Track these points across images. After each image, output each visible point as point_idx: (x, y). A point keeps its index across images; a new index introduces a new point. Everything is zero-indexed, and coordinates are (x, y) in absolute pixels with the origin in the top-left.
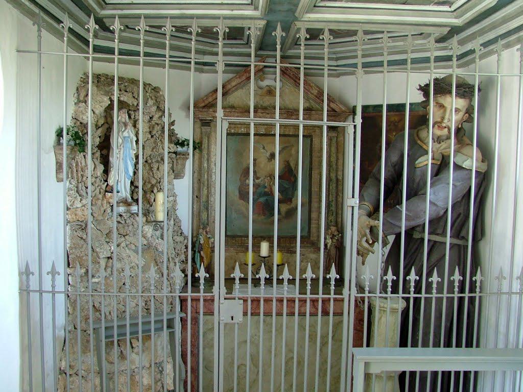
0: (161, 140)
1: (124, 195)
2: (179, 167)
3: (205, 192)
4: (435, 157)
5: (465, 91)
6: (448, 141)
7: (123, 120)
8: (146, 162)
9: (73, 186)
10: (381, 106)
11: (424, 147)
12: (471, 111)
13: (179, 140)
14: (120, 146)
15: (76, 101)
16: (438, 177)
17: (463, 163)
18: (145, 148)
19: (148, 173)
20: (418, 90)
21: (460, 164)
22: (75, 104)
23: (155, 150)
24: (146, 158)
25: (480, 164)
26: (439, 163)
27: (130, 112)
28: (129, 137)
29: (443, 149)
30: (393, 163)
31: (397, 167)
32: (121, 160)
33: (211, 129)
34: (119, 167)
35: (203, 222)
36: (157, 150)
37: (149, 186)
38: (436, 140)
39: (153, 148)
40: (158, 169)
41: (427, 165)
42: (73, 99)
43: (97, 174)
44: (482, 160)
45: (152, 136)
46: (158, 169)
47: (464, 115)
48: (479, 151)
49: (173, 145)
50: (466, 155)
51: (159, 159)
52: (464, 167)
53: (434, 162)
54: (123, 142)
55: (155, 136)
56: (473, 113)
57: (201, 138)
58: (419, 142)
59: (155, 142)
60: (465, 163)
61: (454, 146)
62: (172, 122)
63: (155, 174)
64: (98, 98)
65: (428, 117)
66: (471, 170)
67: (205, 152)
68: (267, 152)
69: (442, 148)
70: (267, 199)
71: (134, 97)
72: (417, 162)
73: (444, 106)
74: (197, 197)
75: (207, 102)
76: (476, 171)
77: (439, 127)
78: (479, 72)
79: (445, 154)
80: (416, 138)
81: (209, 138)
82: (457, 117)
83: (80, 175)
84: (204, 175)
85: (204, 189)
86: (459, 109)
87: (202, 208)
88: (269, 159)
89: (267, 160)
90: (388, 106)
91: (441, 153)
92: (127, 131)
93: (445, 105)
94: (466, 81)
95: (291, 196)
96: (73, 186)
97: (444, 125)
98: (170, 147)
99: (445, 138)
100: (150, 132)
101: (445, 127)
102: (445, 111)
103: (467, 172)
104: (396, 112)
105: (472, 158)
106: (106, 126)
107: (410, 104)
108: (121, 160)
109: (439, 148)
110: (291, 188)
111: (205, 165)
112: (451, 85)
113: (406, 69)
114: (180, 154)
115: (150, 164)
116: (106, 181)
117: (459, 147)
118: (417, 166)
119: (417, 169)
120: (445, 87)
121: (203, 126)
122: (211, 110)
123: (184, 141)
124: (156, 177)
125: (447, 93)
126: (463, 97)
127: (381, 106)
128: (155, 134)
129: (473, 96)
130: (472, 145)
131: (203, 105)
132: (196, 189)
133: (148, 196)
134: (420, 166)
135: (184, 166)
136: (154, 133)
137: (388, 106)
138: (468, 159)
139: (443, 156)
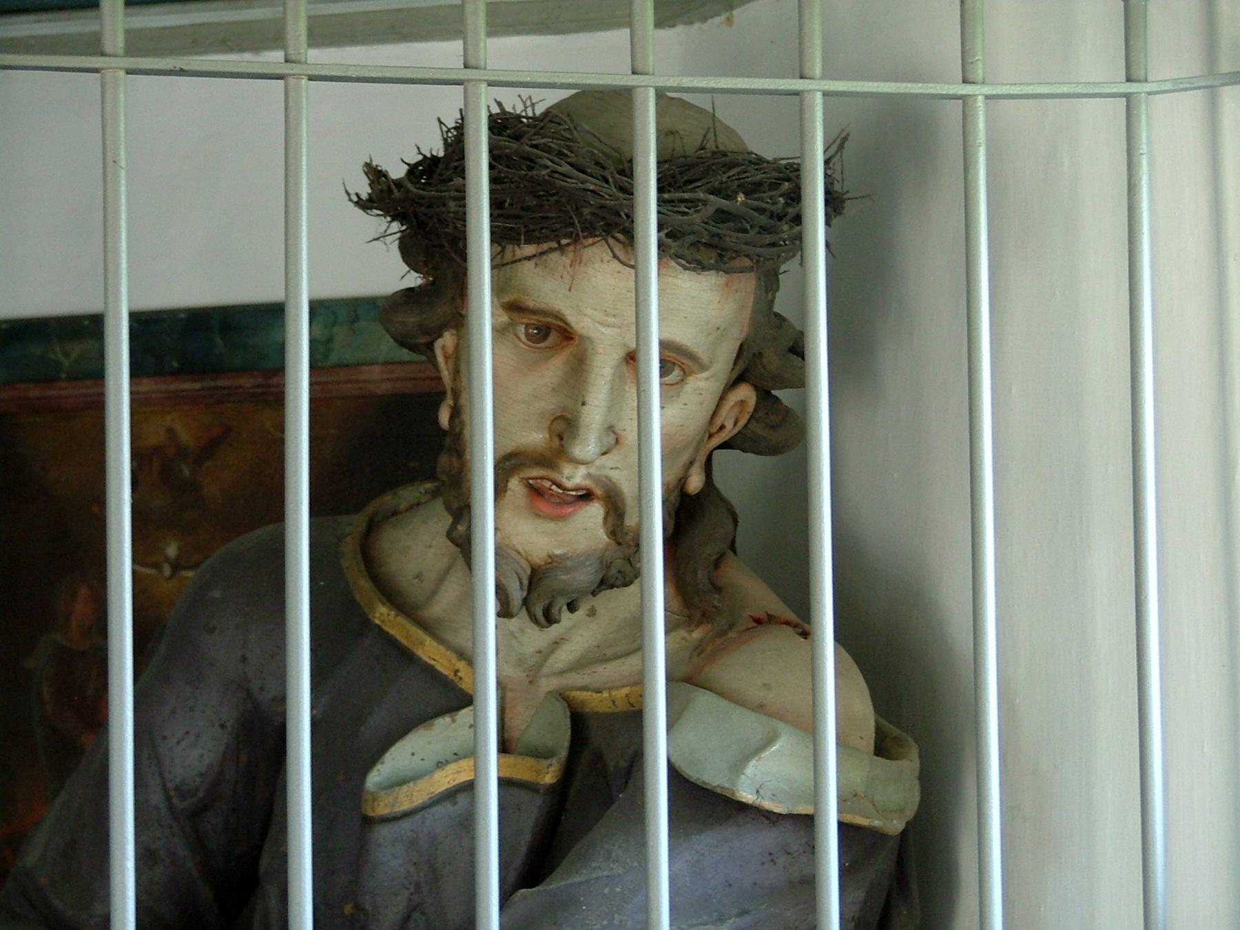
4: (517, 724)
5: (723, 216)
6: (617, 602)
10: (275, 313)
11: (430, 652)
12: (772, 360)
16: (554, 884)
17: (738, 767)
20: (364, 205)
21: (711, 775)
25: (869, 768)
26: (549, 777)
29: (578, 665)
30: (182, 791)
31: (213, 822)
38: (517, 595)
41: (469, 788)
44: (881, 737)
47: (722, 398)
48: (856, 670)
50: (760, 708)
52: (747, 796)
53: (523, 769)
56: (800, 381)
58: (382, 615)
60: (752, 769)
61: (667, 632)
65: (444, 417)
66: (807, 823)
69: (564, 656)
72: (375, 778)
73: (567, 334)
76: (841, 825)
77: (536, 492)
78: (826, 76)
79: (596, 702)
80: (363, 587)
82: (675, 410)
86: (692, 356)
90: (142, 323)
91: (562, 696)
93: (581, 322)
94: (730, 131)
97: (575, 477)
99: (585, 576)
101: (586, 496)
102: (579, 368)
103: (768, 838)
104: (176, 374)
105: (810, 727)
107: (135, 317)
109: (545, 655)
112: (626, 170)
113: (93, 46)
117: (699, 649)
118: (382, 809)
119: (384, 833)
120: (576, 181)
125: (590, 230)
126: (711, 257)
127: (275, 313)
129: (797, 243)
130: (805, 630)
134: (406, 806)
137: (142, 323)
138: (770, 740)
139: (579, 721)
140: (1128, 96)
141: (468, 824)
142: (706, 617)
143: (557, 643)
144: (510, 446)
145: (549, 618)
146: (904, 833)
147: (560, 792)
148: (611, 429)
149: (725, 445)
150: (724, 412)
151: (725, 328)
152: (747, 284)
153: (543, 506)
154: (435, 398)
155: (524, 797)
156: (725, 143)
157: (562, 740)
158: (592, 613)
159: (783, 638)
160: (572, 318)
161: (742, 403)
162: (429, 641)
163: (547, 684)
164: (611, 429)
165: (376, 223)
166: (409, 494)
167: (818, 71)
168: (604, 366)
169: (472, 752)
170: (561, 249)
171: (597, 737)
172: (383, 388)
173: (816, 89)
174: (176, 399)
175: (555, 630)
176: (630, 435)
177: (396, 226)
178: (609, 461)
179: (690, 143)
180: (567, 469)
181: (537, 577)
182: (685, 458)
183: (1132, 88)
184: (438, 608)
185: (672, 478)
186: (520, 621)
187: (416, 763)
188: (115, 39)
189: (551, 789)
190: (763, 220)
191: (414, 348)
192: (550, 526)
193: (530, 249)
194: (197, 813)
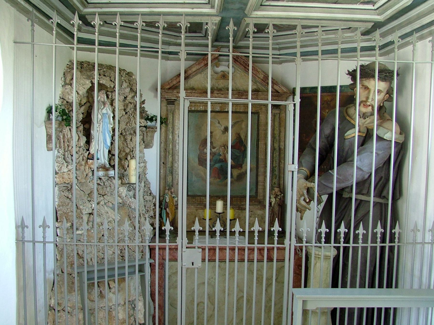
0: (133, 116)
2: (149, 138)
5: (386, 76)
6: (372, 117)
7: (102, 100)
8: (121, 134)
11: (352, 122)
13: (148, 116)
14: (100, 121)
15: (63, 84)
16: (363, 147)
17: (384, 135)
19: (123, 144)
20: (347, 74)
21: (381, 136)
22: (62, 86)
23: (128, 125)
24: (122, 131)
25: (398, 136)
26: (364, 135)
29: (368, 124)
31: (329, 138)
32: (101, 134)
33: (175, 107)
34: (99, 139)
36: (130, 124)
37: (124, 154)
39: (127, 123)
40: (131, 140)
41: (354, 137)
42: (61, 82)
45: (126, 113)
46: (131, 140)
47: (385, 96)
48: (398, 125)
50: (387, 129)
51: (132, 132)
52: (385, 138)
53: (360, 134)
55: (128, 113)
56: (393, 94)
58: (348, 118)
59: (129, 118)
61: (377, 121)
62: (143, 101)
63: (128, 145)
64: (82, 82)
66: (391, 141)
67: (170, 126)
68: (222, 126)
69: (367, 123)
70: (221, 165)
71: (111, 81)
72: (346, 135)
73: (368, 88)
74: (163, 163)
76: (395, 142)
77: (364, 105)
78: (397, 60)
79: (370, 128)
80: (346, 115)
83: (66, 145)
84: (170, 145)
85: (169, 157)
86: (381, 91)
87: (168, 172)
88: (223, 132)
89: (221, 133)
90: (322, 88)
91: (366, 127)
92: (105, 108)
95: (241, 163)
97: (368, 104)
98: (141, 122)
99: (369, 114)
100: (125, 110)
101: (370, 106)
104: (328, 93)
108: (101, 134)
109: (365, 122)
110: (242, 157)
111: (171, 137)
112: (374, 71)
113: (337, 57)
114: (149, 128)
115: (124, 136)
116: (88, 150)
117: (381, 122)
118: (346, 138)
120: (370, 72)
123: (153, 117)
124: (129, 147)
125: (371, 77)
126: (384, 80)
128: (129, 111)
129: (393, 79)
131: (168, 87)
133: (123, 162)
135: (152, 137)
136: (128, 110)
137: (322, 88)
140: (431, 63)
141: (354, 140)
142: (382, 119)
143: (366, 121)
144: (361, 100)
145: (365, 119)
146: (402, 143)
147: (365, 137)
148: (372, 99)
149: (385, 101)
150: (385, 97)
151: (123, 83)
152: (388, 83)
153: (365, 107)
154: (354, 96)
155: (361, 137)
156: (386, 68)
157: (366, 131)
158: (370, 118)
159: (390, 122)
160: (369, 86)
161: (387, 96)
162: (352, 121)
163: (365, 126)
164: (372, 99)
165: (348, 76)
166: (351, 105)
167: (396, 60)
168: (372, 92)
169: (355, 133)
170: (368, 79)
171: (369, 131)
172: (349, 95)
173: (396, 62)
174: (329, 95)
175: (366, 120)
176: (374, 98)
177: (350, 77)
178: (372, 102)
179: (382, 68)
180: (368, 103)
181: (364, 114)
182: (380, 102)
183: (432, 62)
184: (353, 117)
185: (379, 104)
186: (362, 119)
187: (350, 133)
188: (339, 56)
189: (364, 137)
190: (390, 76)
191: (352, 90)
192: (365, 109)
193: (365, 79)
194: (328, 137)
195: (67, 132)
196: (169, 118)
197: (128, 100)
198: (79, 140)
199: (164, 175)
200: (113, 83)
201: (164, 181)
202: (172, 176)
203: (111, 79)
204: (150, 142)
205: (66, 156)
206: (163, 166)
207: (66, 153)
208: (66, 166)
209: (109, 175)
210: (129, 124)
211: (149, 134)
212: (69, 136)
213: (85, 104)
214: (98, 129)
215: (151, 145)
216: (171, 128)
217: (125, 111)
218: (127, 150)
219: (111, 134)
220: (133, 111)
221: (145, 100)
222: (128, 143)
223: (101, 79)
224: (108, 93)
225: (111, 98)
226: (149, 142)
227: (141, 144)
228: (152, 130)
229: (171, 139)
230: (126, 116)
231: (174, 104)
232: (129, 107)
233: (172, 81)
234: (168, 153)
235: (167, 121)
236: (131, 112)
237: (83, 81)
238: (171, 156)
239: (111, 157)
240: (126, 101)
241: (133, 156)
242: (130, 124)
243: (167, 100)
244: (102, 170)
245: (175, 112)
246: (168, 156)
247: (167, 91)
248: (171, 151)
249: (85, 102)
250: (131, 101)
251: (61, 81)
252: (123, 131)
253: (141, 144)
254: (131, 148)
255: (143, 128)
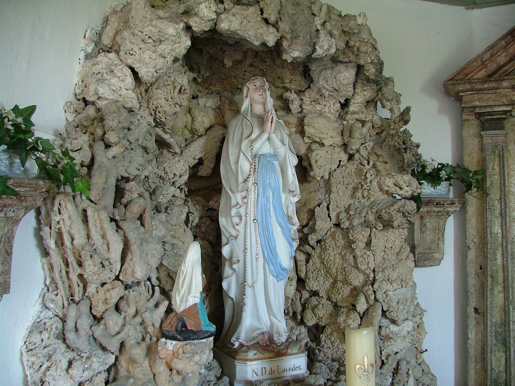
0: (374, 166)
1: (265, 324)
2: (429, 236)
3: (499, 298)
7: (258, 109)
8: (337, 225)
9: (50, 314)
13: (424, 167)
14: (245, 181)
15: (90, 49)
18: (334, 190)
19: (343, 258)
22: (88, 57)
23: (359, 194)
24: (338, 216)
27: (287, 95)
28: (275, 156)
32: (251, 226)
33: (506, 135)
34: (245, 245)
35: (494, 377)
36: (366, 194)
37: (346, 291)
39: (355, 189)
40: (368, 244)
42: (82, 43)
43: (133, 273)
45: (351, 157)
46: (368, 244)
49: (407, 177)
51: (371, 218)
54: (254, 169)
55: (357, 156)
57: (483, 161)
59: (359, 172)
62: (402, 114)
63: (360, 260)
64: (148, 30)
67: (494, 195)
71: (266, 21)
74: (476, 310)
75: (492, 67)
81: (502, 158)
83: (74, 277)
84: (495, 254)
85: (496, 292)
87: (491, 339)
92: (265, 136)
96: (50, 314)
98: (401, 183)
100: (345, 146)
106: (217, 132)
108: (251, 226)
111: (497, 229)
114: (429, 202)
115: (346, 232)
116: (166, 294)
121: (483, 128)
122: (505, 84)
123: (439, 170)
124: (363, 267)
128: (358, 151)
131: (482, 74)
132: (472, 290)
133: (341, 319)
135: (440, 231)
136: (354, 145)
195: (68, 222)
196: (489, 171)
197: (354, 113)
198: (129, 256)
199: (479, 347)
200: (272, 30)
201: (479, 366)
202: (505, 352)
203: (265, 16)
204: (433, 247)
205: (70, 324)
206: (476, 319)
207: (72, 312)
208: (64, 364)
209: (285, 370)
210: (360, 191)
211: (430, 223)
212: (80, 240)
213: (207, 130)
214: (242, 211)
215: (437, 256)
216: (496, 202)
217: (345, 151)
218: (357, 280)
219: (295, 228)
220: (373, 148)
221: (408, 109)
222: (358, 252)
223: (223, 16)
224: (287, 95)
225: (301, 112)
226: (430, 248)
227: (404, 256)
228: (437, 210)
229: (500, 235)
230: (352, 167)
231: (502, 128)
232: (357, 135)
233: (492, 56)
234: (489, 279)
235: (484, 180)
236: (364, 153)
237: (156, 27)
238: (500, 288)
239: (307, 299)
240: (349, 117)
241: (376, 300)
242: (366, 194)
243: (479, 115)
244: (259, 355)
245: (508, 151)
246: (492, 289)
247: (478, 86)
248: (500, 274)
249: (207, 125)
250: (362, 116)
251: (83, 40)
252: (343, 216)
253: (404, 256)
254: (367, 272)
255: (408, 202)
